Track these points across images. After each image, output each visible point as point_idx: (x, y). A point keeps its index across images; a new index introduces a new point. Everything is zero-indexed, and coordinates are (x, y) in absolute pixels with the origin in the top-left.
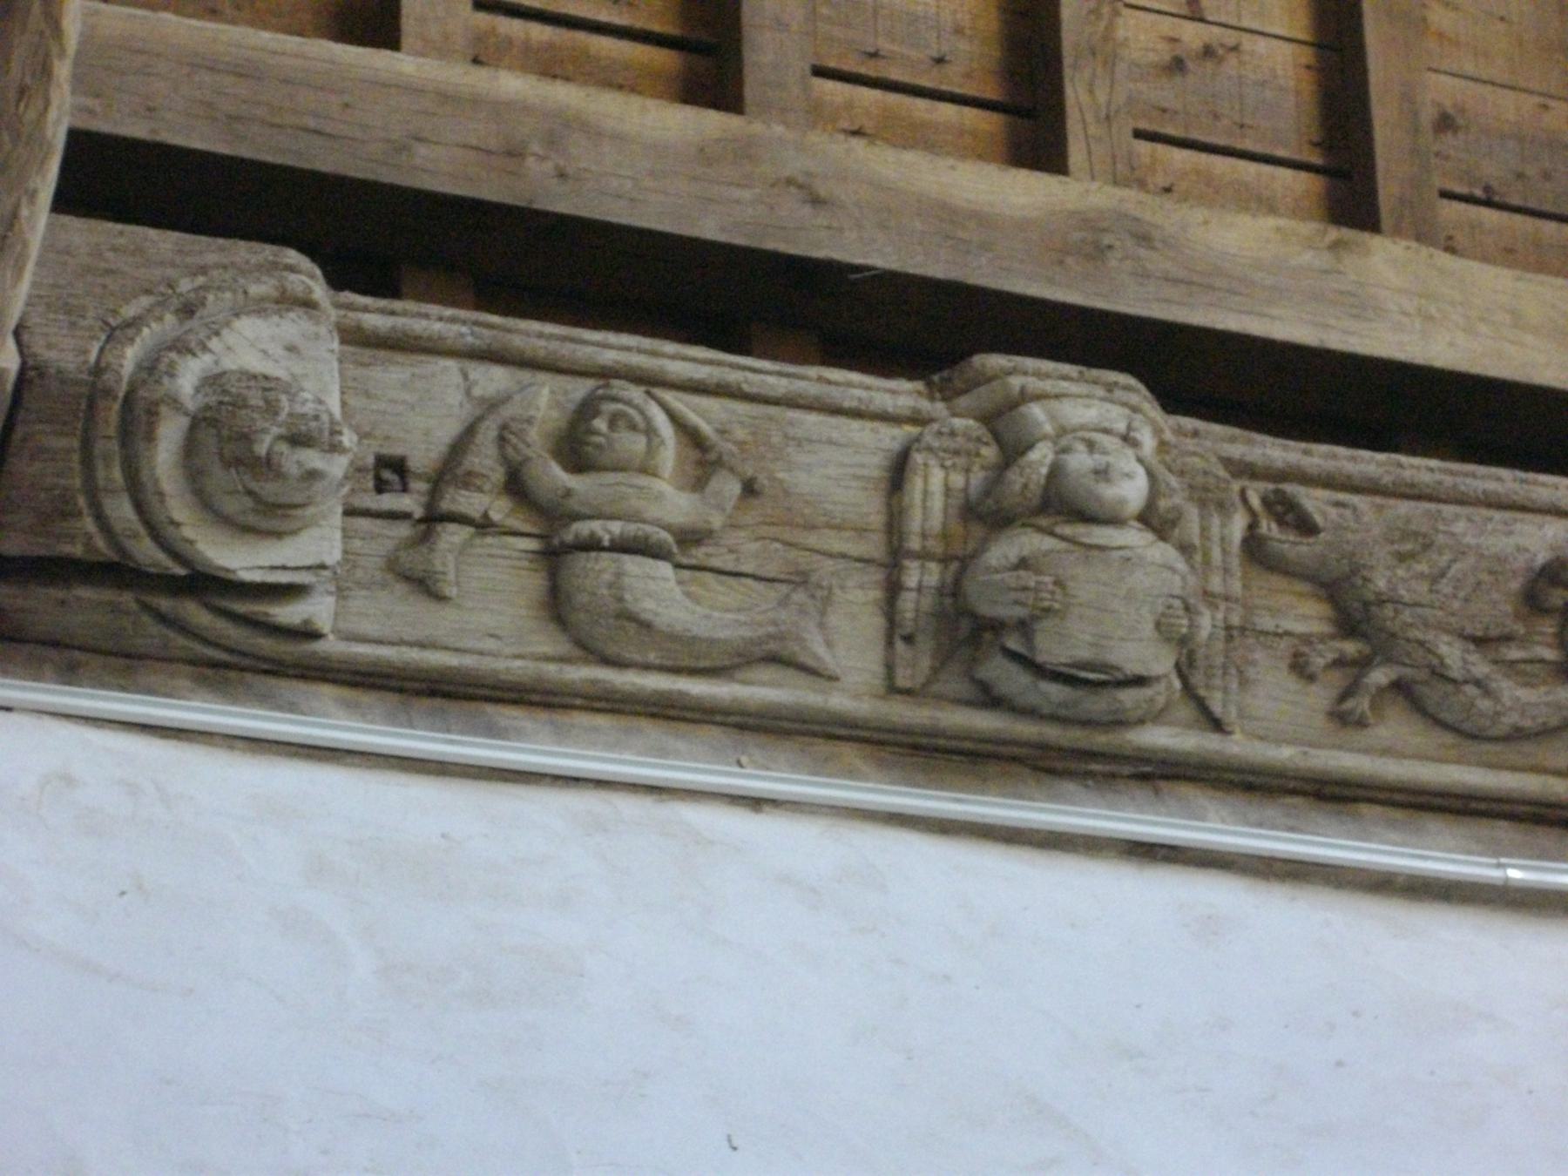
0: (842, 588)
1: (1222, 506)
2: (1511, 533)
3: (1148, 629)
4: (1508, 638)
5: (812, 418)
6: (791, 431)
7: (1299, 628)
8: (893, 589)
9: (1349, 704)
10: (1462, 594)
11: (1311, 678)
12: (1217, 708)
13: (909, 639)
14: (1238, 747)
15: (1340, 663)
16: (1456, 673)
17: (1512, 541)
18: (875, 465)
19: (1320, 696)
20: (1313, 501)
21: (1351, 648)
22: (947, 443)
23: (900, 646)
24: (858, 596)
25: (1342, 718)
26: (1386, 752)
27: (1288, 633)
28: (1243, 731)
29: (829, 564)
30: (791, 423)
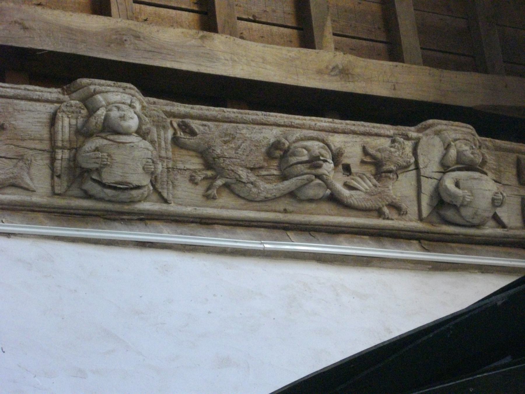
0: (35, 160)
1: (164, 127)
2: (262, 133)
3: (140, 170)
4: (261, 168)
5: (23, 102)
6: (16, 107)
7: (192, 167)
8: (53, 159)
9: (210, 192)
10: (245, 154)
11: (196, 184)
12: (165, 195)
13: (59, 177)
14: (173, 208)
15: (206, 178)
16: (244, 180)
17: (262, 135)
18: (45, 117)
19: (200, 189)
20: (195, 124)
21: (209, 173)
22: (69, 109)
23: (56, 179)
24: (41, 162)
25: (207, 197)
26: (222, 207)
27: (188, 169)
28: (174, 202)
29: (31, 152)
30: (16, 105)
